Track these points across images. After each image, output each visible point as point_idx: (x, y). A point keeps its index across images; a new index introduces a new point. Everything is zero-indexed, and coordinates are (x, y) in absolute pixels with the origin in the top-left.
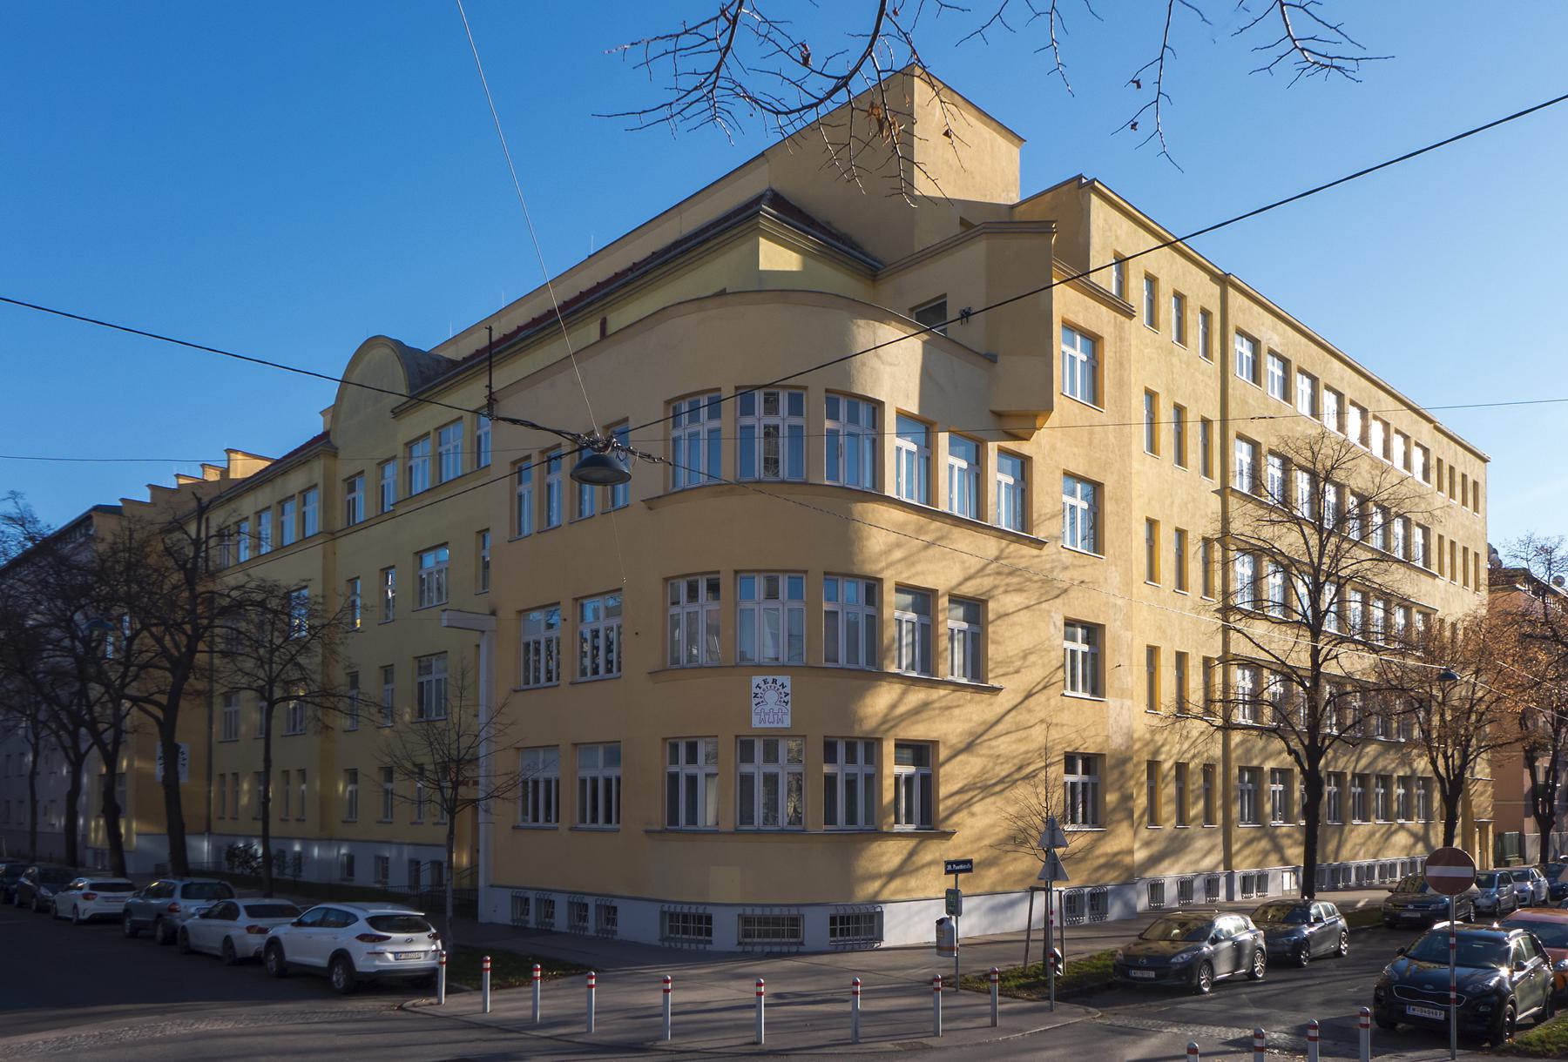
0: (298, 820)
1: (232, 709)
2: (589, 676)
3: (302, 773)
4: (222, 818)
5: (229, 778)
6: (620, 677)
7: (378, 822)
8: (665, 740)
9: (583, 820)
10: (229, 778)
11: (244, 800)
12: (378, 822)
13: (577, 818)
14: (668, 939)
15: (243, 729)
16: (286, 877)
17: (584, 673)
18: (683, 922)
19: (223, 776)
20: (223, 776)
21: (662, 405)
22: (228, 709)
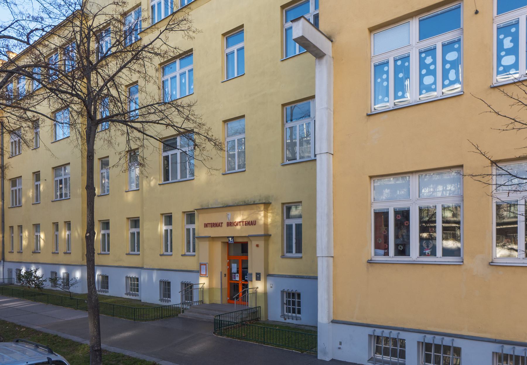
0: (65, 253)
1: (17, 188)
2: (59, 199)
3: (68, 224)
4: (11, 252)
5: (16, 229)
6: (70, 198)
7: (127, 254)
8: (283, 204)
9: (188, 250)
10: (16, 229)
11: (24, 243)
12: (127, 254)
13: (67, 250)
14: (185, 303)
15: (23, 200)
16: (58, 289)
17: (56, 196)
18: (293, 306)
19: (12, 228)
20: (12, 228)
21: (279, 9)
22: (14, 189)
